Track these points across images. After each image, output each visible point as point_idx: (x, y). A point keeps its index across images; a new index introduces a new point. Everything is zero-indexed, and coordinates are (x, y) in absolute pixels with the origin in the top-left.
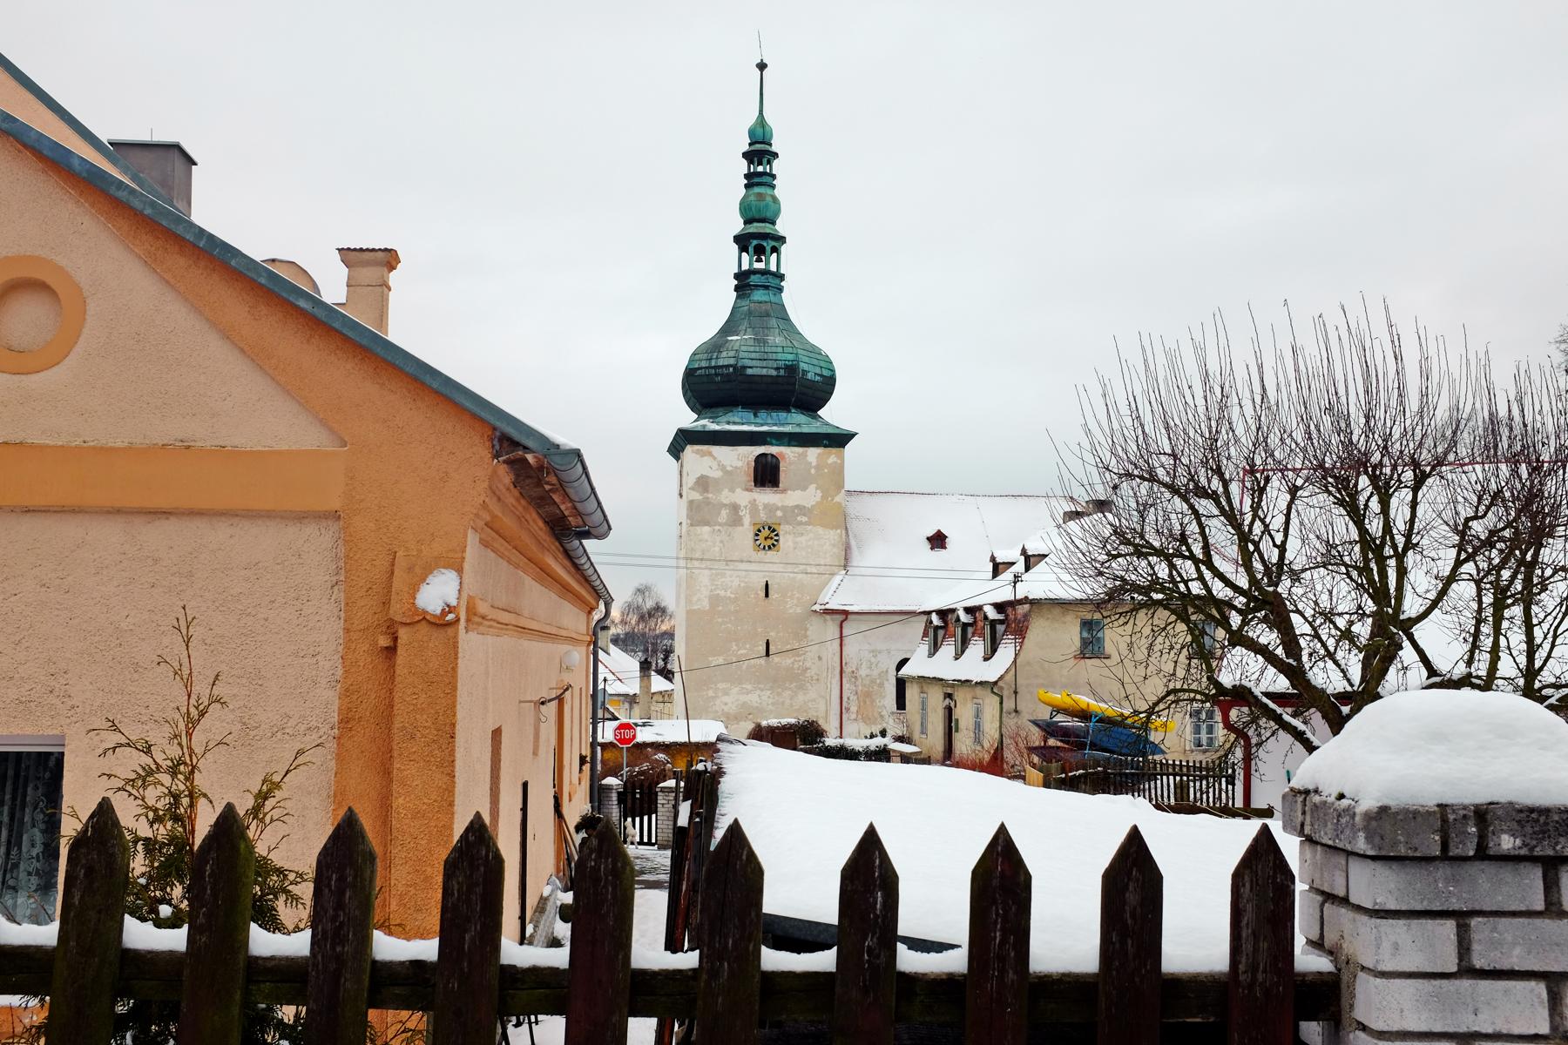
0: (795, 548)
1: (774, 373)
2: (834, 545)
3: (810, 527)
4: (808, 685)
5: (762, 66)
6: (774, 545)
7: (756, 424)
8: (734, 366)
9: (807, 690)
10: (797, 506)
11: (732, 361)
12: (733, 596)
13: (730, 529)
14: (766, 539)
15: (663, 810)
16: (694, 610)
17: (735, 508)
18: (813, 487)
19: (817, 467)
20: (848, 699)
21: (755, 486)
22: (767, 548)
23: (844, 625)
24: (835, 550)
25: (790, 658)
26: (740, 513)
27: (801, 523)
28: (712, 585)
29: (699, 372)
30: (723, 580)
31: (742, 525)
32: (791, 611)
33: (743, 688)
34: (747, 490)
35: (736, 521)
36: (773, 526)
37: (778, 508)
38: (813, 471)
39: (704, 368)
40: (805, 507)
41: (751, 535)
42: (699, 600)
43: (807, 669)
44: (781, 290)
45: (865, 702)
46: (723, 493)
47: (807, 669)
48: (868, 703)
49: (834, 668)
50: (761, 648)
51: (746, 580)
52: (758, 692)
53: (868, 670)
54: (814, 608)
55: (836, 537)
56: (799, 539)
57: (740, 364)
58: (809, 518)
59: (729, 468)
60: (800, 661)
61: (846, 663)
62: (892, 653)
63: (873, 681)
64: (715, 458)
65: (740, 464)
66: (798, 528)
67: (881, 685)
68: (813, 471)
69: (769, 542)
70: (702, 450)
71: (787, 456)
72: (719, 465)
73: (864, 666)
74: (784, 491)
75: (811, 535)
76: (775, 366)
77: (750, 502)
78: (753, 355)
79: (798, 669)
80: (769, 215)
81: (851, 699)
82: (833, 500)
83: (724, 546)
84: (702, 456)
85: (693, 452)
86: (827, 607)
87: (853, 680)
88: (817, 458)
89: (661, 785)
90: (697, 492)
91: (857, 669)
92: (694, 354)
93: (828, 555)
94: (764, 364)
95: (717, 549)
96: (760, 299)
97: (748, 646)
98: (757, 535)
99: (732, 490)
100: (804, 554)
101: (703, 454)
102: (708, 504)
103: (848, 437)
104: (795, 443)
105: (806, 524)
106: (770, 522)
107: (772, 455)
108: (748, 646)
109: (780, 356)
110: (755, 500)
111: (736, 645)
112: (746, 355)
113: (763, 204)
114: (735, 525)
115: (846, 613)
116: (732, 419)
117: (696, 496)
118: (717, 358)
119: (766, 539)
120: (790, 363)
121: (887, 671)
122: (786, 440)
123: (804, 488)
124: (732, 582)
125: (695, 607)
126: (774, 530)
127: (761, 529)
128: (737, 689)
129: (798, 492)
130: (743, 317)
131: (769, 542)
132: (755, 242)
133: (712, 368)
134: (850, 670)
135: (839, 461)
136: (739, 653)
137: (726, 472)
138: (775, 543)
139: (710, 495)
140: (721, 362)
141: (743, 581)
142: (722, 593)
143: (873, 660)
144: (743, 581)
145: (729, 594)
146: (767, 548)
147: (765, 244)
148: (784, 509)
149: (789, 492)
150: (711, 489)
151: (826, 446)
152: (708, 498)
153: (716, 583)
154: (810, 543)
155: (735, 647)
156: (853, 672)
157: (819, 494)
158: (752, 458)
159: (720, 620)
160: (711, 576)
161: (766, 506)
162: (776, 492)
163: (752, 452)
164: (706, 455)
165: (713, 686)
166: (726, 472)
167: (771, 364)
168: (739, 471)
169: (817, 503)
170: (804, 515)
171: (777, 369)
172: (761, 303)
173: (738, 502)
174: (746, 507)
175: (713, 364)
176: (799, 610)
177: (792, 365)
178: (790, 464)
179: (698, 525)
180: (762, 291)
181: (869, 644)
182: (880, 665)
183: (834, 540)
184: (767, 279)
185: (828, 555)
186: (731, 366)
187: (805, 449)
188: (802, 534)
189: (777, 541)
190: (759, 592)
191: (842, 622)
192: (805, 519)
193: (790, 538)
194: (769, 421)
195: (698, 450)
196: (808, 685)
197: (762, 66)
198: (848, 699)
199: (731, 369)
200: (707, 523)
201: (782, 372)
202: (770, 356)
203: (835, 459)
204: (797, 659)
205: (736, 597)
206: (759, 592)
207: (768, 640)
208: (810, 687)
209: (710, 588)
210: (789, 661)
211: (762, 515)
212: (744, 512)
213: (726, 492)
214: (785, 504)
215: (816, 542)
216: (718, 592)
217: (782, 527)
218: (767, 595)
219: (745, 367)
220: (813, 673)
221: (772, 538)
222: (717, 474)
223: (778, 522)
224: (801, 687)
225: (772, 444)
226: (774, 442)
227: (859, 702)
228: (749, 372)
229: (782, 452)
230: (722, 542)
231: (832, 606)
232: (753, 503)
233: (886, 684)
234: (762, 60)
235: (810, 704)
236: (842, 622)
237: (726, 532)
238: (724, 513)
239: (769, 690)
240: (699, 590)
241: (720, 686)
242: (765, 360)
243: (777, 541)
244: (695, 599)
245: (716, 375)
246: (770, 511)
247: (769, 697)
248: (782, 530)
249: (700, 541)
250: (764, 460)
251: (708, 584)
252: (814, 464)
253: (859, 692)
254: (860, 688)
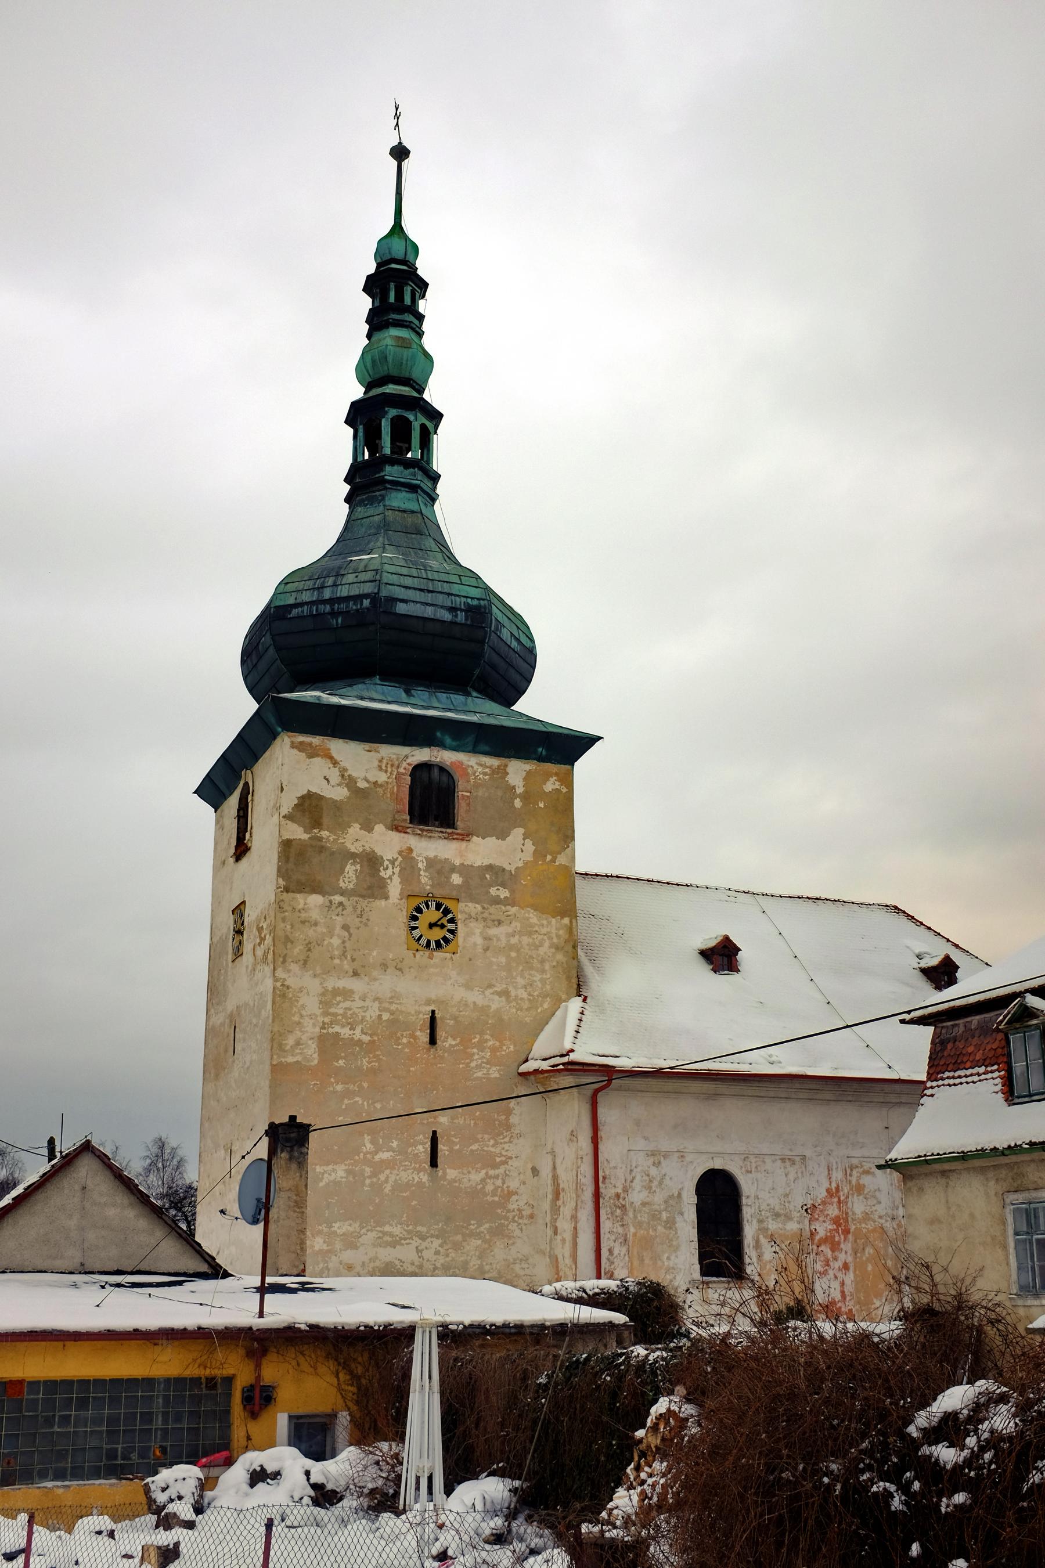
0: (486, 949)
1: (447, 616)
2: (557, 948)
3: (514, 910)
4: (513, 1226)
5: (400, 153)
6: (445, 939)
7: (413, 705)
8: (374, 598)
9: (510, 1237)
10: (490, 868)
11: (368, 588)
12: (366, 1039)
13: (363, 903)
14: (431, 926)
15: (54, 1538)
16: (289, 1064)
17: (371, 861)
18: (518, 833)
19: (526, 797)
20: (610, 1251)
21: (411, 822)
22: (433, 945)
23: (600, 1096)
24: (560, 957)
25: (478, 1171)
26: (382, 874)
27: (497, 901)
28: (326, 1014)
29: (295, 612)
30: (347, 1004)
31: (387, 898)
32: (479, 1074)
33: (385, 1233)
34: (396, 828)
35: (376, 888)
36: (447, 903)
37: (453, 869)
38: (518, 803)
39: (307, 603)
40: (504, 870)
41: (403, 917)
42: (298, 1043)
43: (511, 1193)
44: (433, 499)
45: (642, 1260)
46: (351, 830)
47: (511, 1193)
48: (647, 1261)
49: (578, 1187)
50: (420, 1148)
51: (393, 1007)
52: (416, 1242)
53: (645, 1193)
54: (524, 1068)
55: (561, 932)
56: (493, 931)
57: (384, 593)
58: (512, 891)
59: (362, 784)
60: (497, 1177)
61: (604, 1178)
62: (689, 1158)
63: (655, 1216)
64: (335, 763)
65: (382, 778)
66: (492, 909)
67: (670, 1224)
68: (518, 803)
69: (437, 934)
70: (310, 744)
71: (470, 770)
72: (343, 776)
73: (637, 1184)
74: (465, 837)
75: (517, 925)
76: (449, 604)
77: (400, 853)
78: (408, 582)
79: (494, 1194)
80: (416, 375)
81: (616, 1252)
82: (553, 861)
83: (350, 935)
84: (311, 756)
85: (293, 746)
86: (573, 1057)
87: (618, 1211)
88: (525, 779)
89: (922, 1419)
90: (300, 824)
91: (625, 1190)
92: (284, 582)
93: (547, 967)
94: (429, 598)
95: (336, 941)
96: (403, 506)
97: (395, 1144)
98: (415, 919)
99: (368, 827)
100: (503, 960)
101: (312, 753)
102: (322, 849)
103: (586, 742)
104: (486, 748)
105: (505, 902)
106: (438, 892)
107: (442, 769)
108: (395, 1144)
109: (456, 589)
110: (410, 850)
111: (372, 1142)
112: (394, 579)
113: (406, 353)
114: (373, 896)
115: (609, 1072)
116: (365, 694)
117: (297, 832)
118: (335, 585)
119: (431, 926)
120: (475, 602)
121: (679, 1195)
122: (470, 739)
123: (502, 835)
124: (366, 1009)
125: (290, 1059)
126: (447, 911)
127: (423, 907)
128: (372, 1235)
129: (492, 841)
130: (373, 531)
131: (437, 934)
132: (393, 412)
133: (324, 602)
134: (612, 1192)
135: (565, 790)
136: (377, 1158)
137: (356, 792)
138: (449, 936)
139: (325, 834)
140: (343, 592)
141: (386, 1010)
142: (345, 1032)
143: (654, 1171)
144: (386, 1010)
145: (358, 1034)
146: (433, 945)
147: (411, 417)
148: (465, 870)
149: (475, 838)
150: (326, 820)
151: (541, 759)
152: (320, 839)
153: (332, 1010)
154: (514, 941)
155: (369, 1146)
156: (618, 1196)
157: (530, 847)
158: (405, 768)
159: (339, 1088)
160: (323, 994)
161: (431, 863)
162: (450, 837)
163: (407, 757)
164: (318, 755)
165: (324, 1228)
166: (356, 792)
167: (440, 599)
168: (380, 790)
169: (526, 863)
170: (503, 885)
171: (452, 609)
172: (404, 511)
173: (379, 851)
174: (393, 862)
175: (327, 594)
176: (494, 1073)
177: (478, 607)
178: (477, 786)
179: (300, 892)
180: (404, 494)
181: (646, 1138)
182: (667, 1181)
183: (558, 936)
184: (415, 475)
185: (547, 967)
186: (366, 596)
187: (504, 761)
188: (500, 922)
189: (452, 932)
190: (418, 1033)
191: (596, 1092)
192: (504, 893)
193: (477, 928)
194: (437, 705)
195: (301, 743)
196: (513, 1226)
197: (400, 153)
198: (610, 1251)
199: (366, 603)
200: (316, 888)
201: (461, 617)
202: (439, 587)
203: (557, 785)
204: (492, 1172)
205: (372, 1042)
206: (418, 1033)
207: (434, 1133)
208: (517, 1232)
209: (321, 1019)
210: (476, 1177)
211: (424, 880)
212: (389, 872)
213: (355, 830)
214: (468, 862)
215: (526, 940)
216: (337, 1029)
217: (461, 905)
218: (433, 1041)
219: (393, 600)
220: (522, 1203)
221: (443, 926)
222: (339, 793)
223: (454, 894)
224: (499, 1232)
225: (441, 745)
226: (448, 741)
227: (631, 1261)
228: (401, 608)
229: (461, 763)
230: (346, 927)
231: (582, 1054)
232: (407, 854)
233: (680, 1224)
234: (400, 143)
235: (517, 1267)
236: (596, 1092)
237: (355, 908)
238: (351, 870)
239: (437, 1237)
240: (299, 1023)
241: (341, 1227)
242: (429, 591)
243: (452, 932)
244: (290, 1041)
245: (333, 614)
246: (439, 872)
247: (437, 1253)
248: (463, 909)
249: (303, 922)
250: (425, 775)
251: (319, 1012)
252: (520, 790)
253: (630, 1237)
254: (632, 1230)
